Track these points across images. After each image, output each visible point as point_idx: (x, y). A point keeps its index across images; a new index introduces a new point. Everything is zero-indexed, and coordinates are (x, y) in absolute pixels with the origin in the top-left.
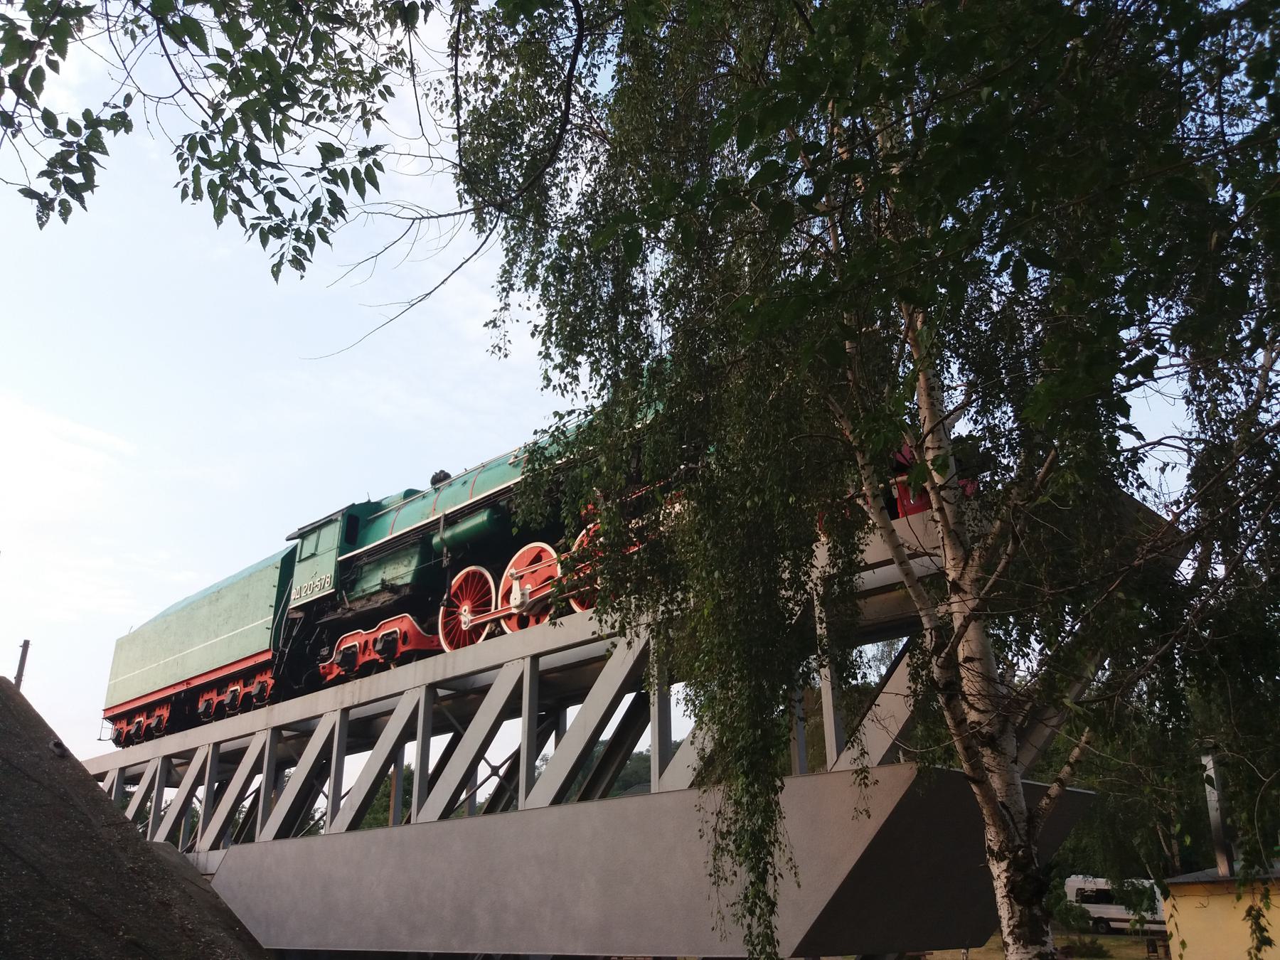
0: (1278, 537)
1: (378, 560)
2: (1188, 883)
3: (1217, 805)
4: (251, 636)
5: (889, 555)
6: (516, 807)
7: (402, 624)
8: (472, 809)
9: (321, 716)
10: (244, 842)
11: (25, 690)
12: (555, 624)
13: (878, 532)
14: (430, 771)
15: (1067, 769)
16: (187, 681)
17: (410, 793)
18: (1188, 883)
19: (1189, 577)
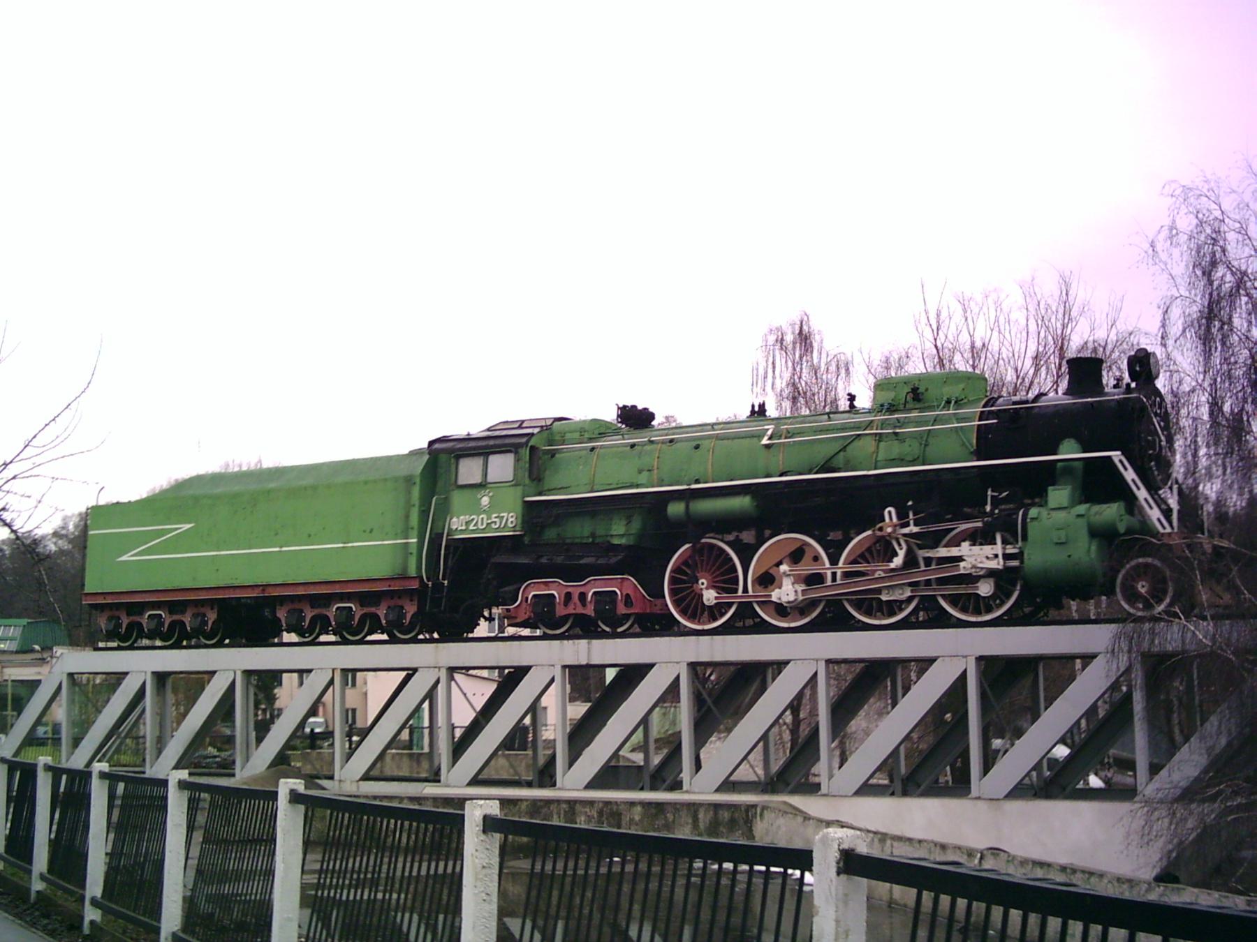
0: (387, 855)
1: (520, 427)
2: (247, 727)
3: (1216, 895)
4: (374, 550)
5: (490, 479)
6: (572, 700)
7: (620, 586)
8: (1034, 769)
9: (310, 671)
10: (935, 790)
11: (467, 724)
12: (777, 329)
13: (970, 370)
14: (608, 682)
15: (716, 867)
16: (265, 587)
17: (781, 475)
18: (247, 727)
19: (1116, 505)
